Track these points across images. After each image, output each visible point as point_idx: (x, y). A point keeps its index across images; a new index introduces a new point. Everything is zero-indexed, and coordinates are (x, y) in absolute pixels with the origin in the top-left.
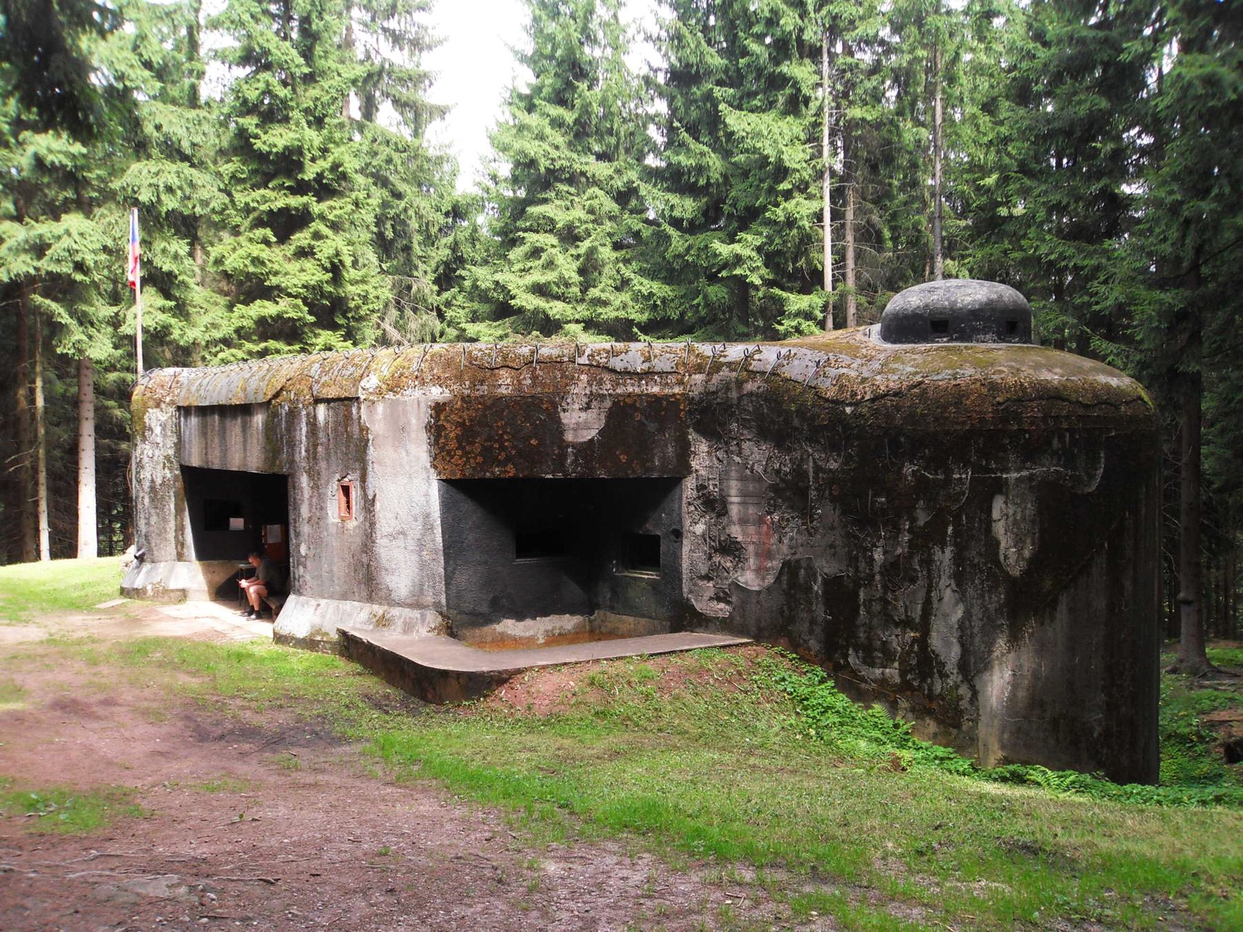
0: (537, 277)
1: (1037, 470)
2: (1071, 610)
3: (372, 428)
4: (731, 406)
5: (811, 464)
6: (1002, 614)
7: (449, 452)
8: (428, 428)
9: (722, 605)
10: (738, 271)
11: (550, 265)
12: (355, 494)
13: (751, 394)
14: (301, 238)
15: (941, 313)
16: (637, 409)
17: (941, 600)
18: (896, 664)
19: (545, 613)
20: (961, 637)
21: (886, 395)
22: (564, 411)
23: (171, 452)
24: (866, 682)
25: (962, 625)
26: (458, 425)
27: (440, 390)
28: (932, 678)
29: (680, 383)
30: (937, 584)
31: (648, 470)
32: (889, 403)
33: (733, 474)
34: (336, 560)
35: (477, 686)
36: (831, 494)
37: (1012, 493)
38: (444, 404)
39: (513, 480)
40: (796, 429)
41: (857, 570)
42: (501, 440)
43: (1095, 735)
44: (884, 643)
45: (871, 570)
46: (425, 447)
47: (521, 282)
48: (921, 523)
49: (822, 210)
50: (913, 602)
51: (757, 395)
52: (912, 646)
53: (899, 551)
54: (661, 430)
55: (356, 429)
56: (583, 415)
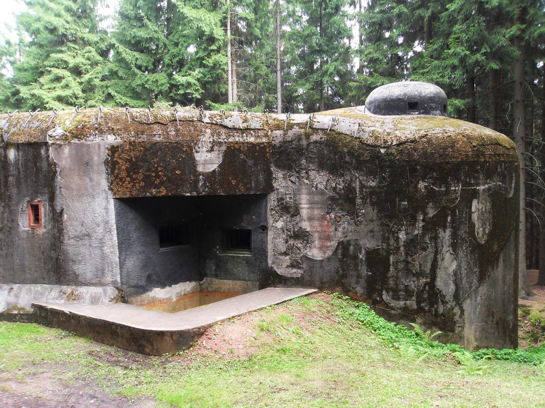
0: (60, 92)
1: (492, 184)
2: (504, 260)
3: (59, 163)
4: (302, 149)
5: (358, 183)
6: (476, 265)
7: (121, 180)
8: (106, 163)
9: (295, 270)
10: (188, 91)
11: (67, 86)
13: (316, 142)
15: (414, 98)
16: (241, 152)
17: (443, 259)
18: (414, 298)
20: (455, 280)
21: (406, 142)
22: (197, 152)
24: (394, 309)
25: (455, 274)
26: (127, 160)
28: (437, 304)
29: (266, 136)
30: (441, 250)
31: (249, 189)
32: (409, 147)
33: (304, 191)
34: (27, 256)
35: (184, 340)
36: (371, 201)
37: (481, 198)
38: (118, 147)
39: (165, 197)
40: (348, 163)
41: (388, 245)
42: (157, 172)
44: (406, 286)
45: (397, 244)
46: (104, 176)
47: (49, 95)
48: (431, 215)
50: (425, 261)
51: (320, 143)
53: (416, 232)
55: (45, 165)
56: (209, 155)
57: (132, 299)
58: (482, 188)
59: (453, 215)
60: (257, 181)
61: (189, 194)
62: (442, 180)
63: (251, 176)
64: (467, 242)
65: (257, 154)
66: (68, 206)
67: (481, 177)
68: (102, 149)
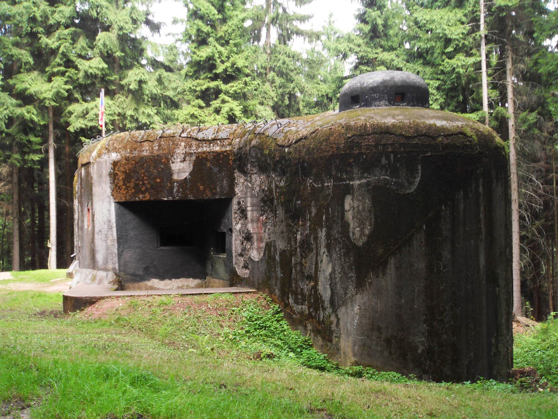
1: (372, 179)
2: (397, 268)
6: (352, 269)
7: (119, 187)
12: (90, 210)
13: (254, 146)
14: (215, 104)
15: (356, 91)
16: (207, 160)
17: (322, 261)
19: (177, 277)
22: (173, 163)
27: (116, 154)
28: (319, 310)
29: (230, 144)
31: (214, 194)
38: (117, 162)
42: (143, 180)
43: (419, 351)
44: (302, 289)
46: (109, 185)
49: (480, 62)
52: (311, 291)
54: (220, 171)
56: (182, 164)
57: (129, 284)
60: (222, 187)
61: (166, 199)
63: (216, 182)
64: (340, 243)
65: (221, 162)
67: (355, 170)
68: (108, 163)
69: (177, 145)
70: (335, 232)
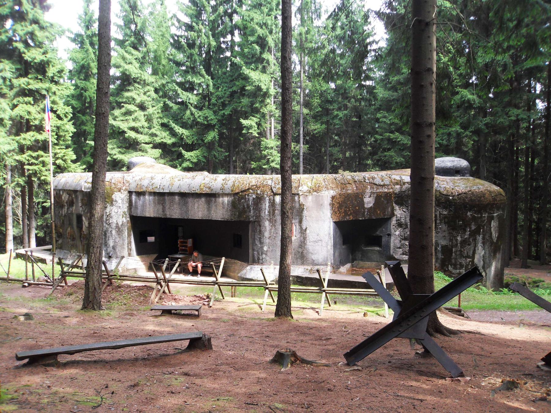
0: (133, 124)
8: (330, 204)
9: (404, 256)
23: (126, 210)
29: (392, 188)
31: (384, 215)
41: (452, 243)
48: (473, 229)
53: (466, 237)
55: (297, 205)
58: (495, 215)
59: (483, 229)
62: (479, 212)
66: (310, 226)
69: (366, 188)
70: (487, 237)
